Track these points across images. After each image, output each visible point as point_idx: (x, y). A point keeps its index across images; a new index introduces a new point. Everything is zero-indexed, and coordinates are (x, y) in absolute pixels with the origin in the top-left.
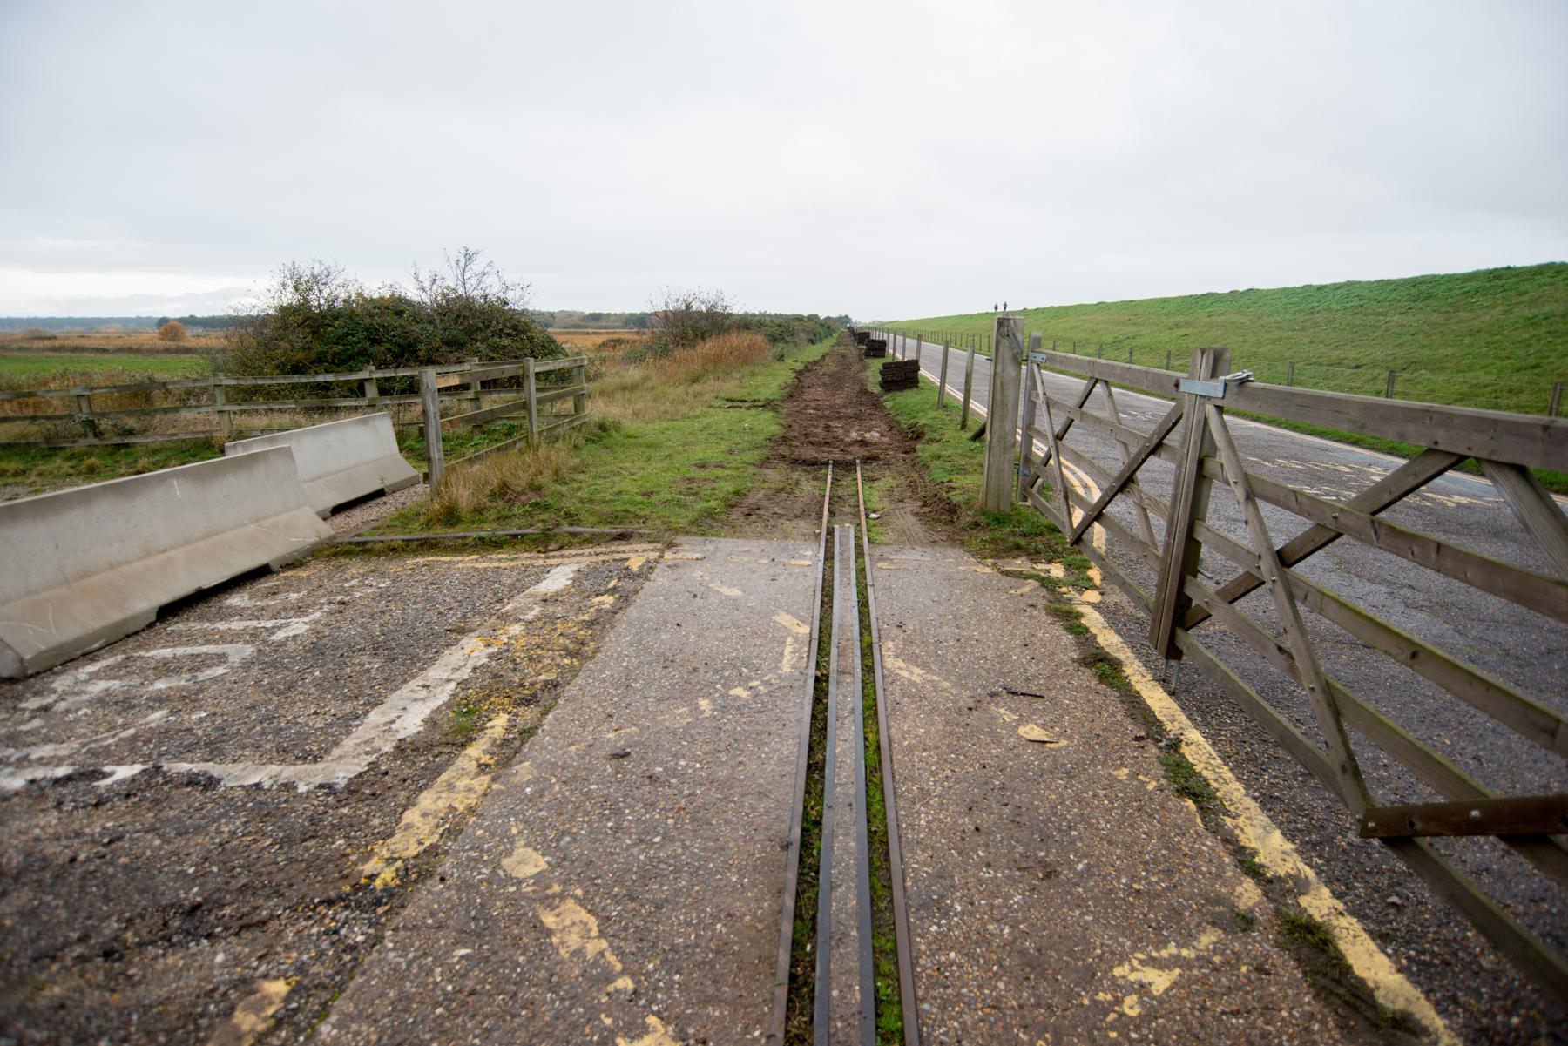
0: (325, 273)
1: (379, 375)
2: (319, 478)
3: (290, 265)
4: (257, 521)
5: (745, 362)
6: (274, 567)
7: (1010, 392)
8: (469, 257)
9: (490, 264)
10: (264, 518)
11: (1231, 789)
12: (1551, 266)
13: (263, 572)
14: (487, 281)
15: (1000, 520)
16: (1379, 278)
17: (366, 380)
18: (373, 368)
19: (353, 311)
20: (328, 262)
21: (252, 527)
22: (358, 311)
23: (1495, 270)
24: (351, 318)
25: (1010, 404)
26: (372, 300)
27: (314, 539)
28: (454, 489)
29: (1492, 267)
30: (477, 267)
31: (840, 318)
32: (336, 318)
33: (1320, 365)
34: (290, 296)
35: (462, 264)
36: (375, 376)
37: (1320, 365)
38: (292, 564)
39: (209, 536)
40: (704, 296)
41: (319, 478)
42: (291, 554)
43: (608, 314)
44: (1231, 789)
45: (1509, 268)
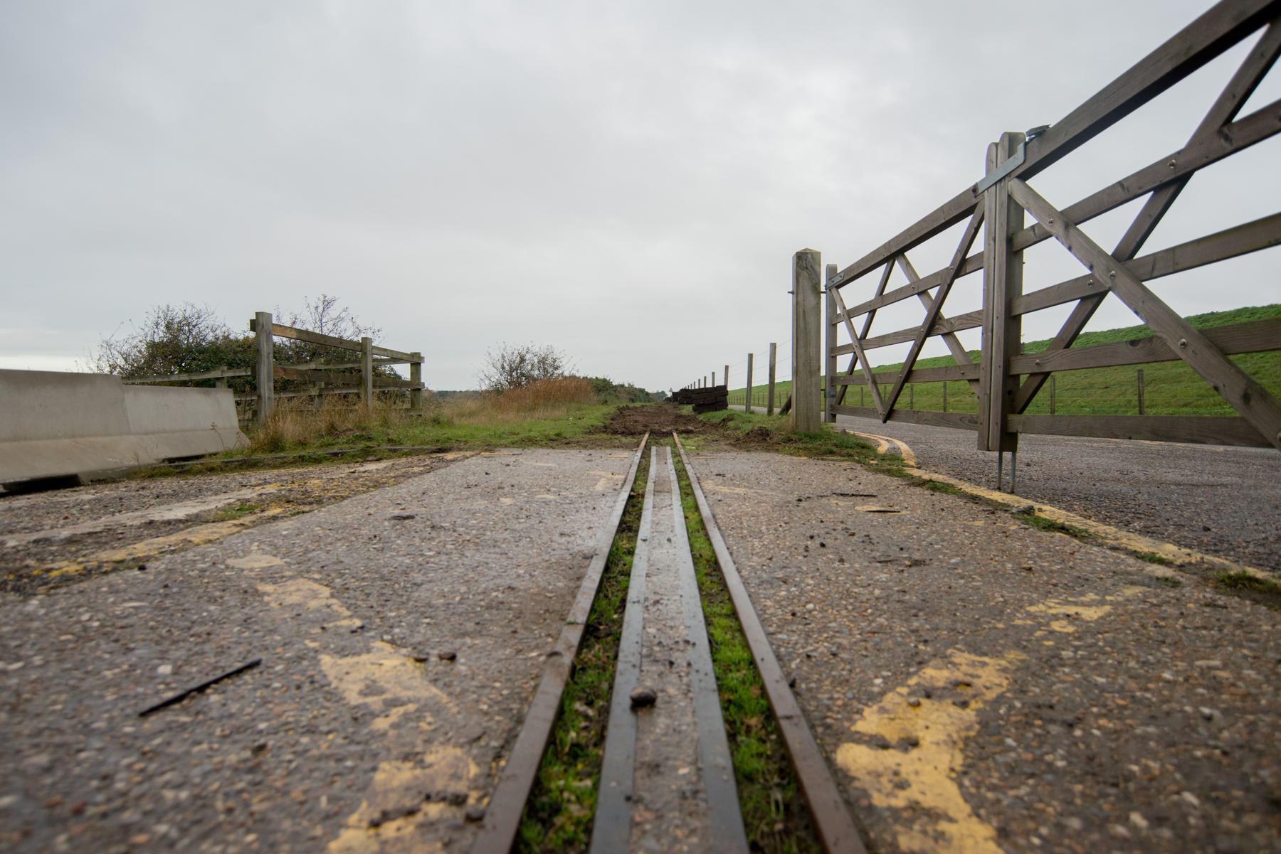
0: (196, 315)
1: (231, 374)
2: (153, 433)
3: (164, 308)
4: (73, 436)
5: (571, 400)
6: (83, 479)
7: (811, 319)
8: (327, 304)
9: (345, 310)
10: (82, 436)
11: (1094, 526)
12: (1245, 309)
13: (69, 482)
14: (343, 325)
15: (813, 437)
16: (1111, 328)
17: (218, 379)
18: (225, 368)
19: (218, 348)
20: (199, 306)
21: (67, 441)
22: (223, 348)
23: (1203, 315)
24: (215, 353)
25: (813, 331)
26: (237, 341)
27: (133, 463)
28: (281, 424)
29: (1200, 313)
30: (333, 312)
31: (658, 394)
32: (201, 352)
33: (1075, 389)
34: (161, 334)
35: (320, 310)
36: (226, 375)
37: (1075, 389)
38: (101, 479)
39: (16, 439)
40: (536, 349)
41: (153, 433)
42: (104, 471)
43: (454, 392)
44: (1094, 526)
45: (1212, 313)
